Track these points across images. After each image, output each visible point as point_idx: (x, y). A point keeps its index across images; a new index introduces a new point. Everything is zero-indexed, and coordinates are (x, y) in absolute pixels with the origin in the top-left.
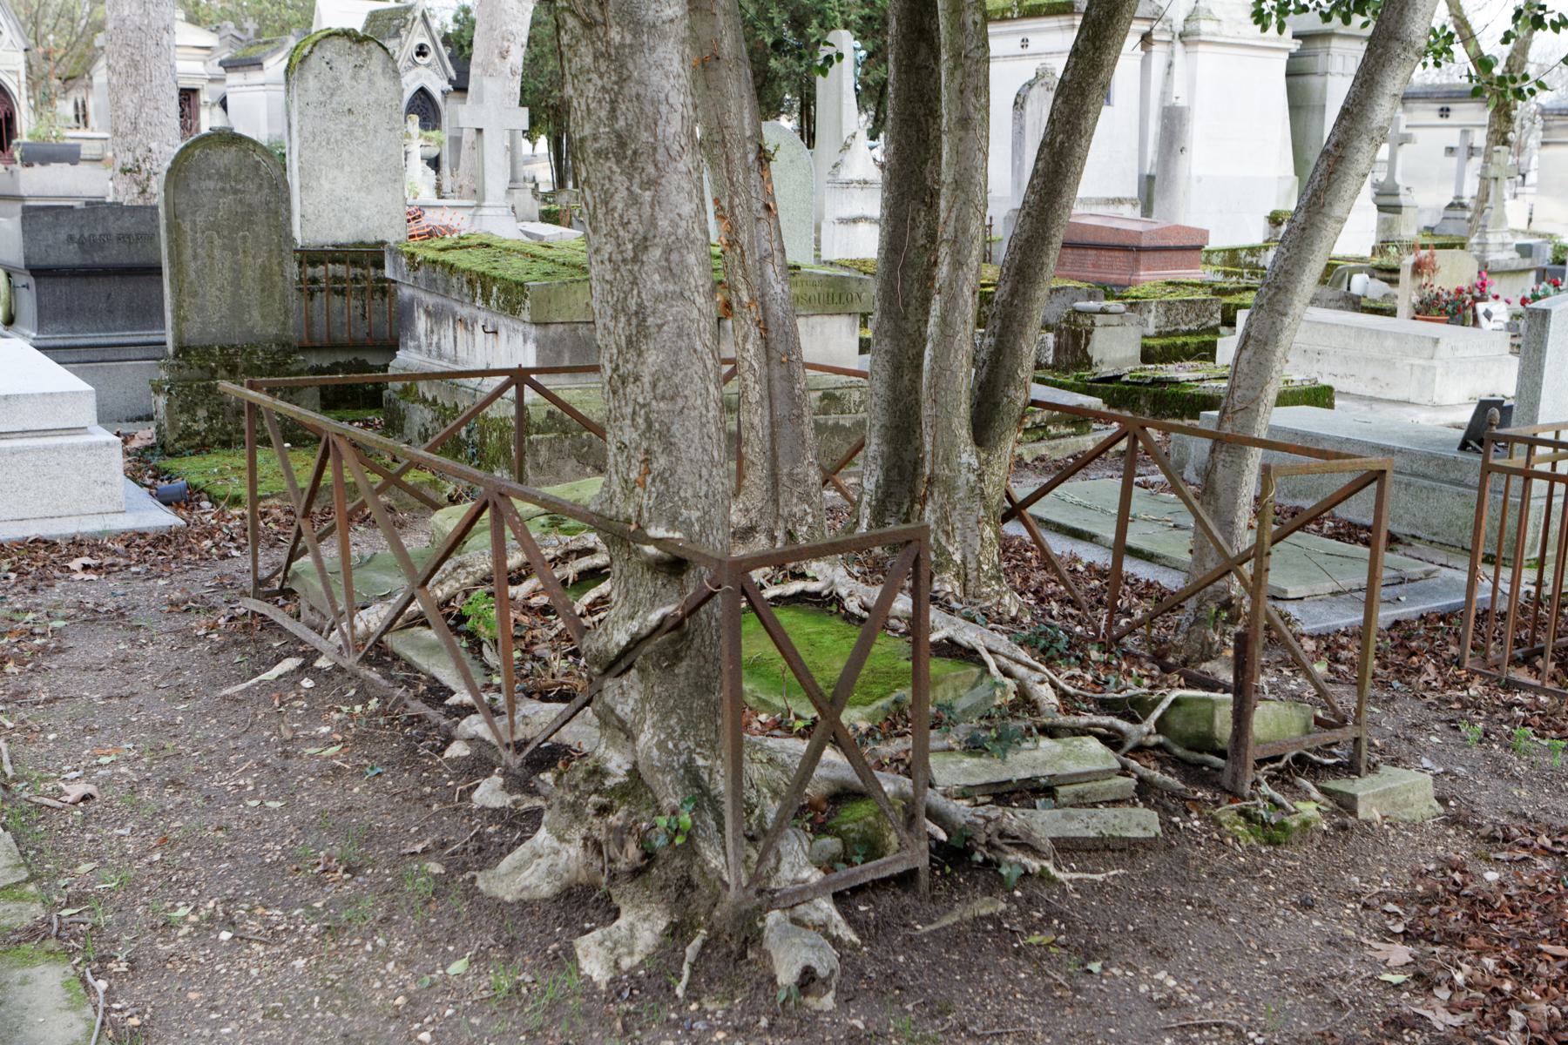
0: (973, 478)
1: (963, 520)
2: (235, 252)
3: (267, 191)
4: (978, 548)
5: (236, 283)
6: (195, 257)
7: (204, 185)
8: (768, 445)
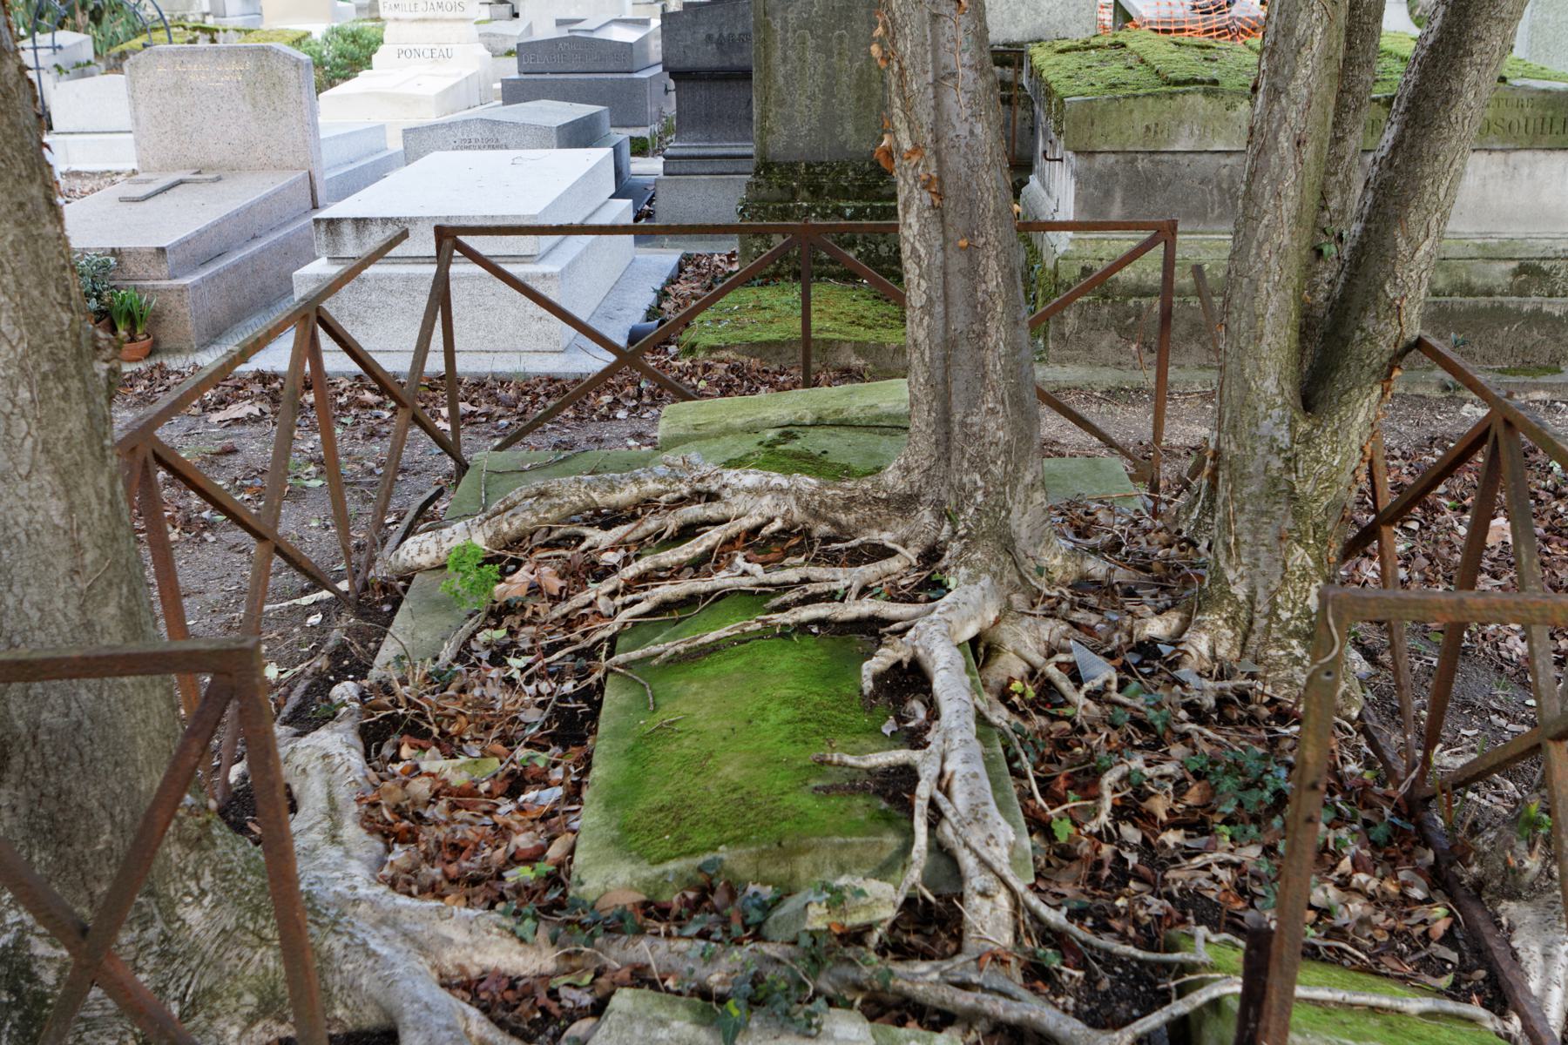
0: (1277, 463)
1: (1255, 532)
4: (1277, 582)
6: (785, 60)
8: (939, 374)
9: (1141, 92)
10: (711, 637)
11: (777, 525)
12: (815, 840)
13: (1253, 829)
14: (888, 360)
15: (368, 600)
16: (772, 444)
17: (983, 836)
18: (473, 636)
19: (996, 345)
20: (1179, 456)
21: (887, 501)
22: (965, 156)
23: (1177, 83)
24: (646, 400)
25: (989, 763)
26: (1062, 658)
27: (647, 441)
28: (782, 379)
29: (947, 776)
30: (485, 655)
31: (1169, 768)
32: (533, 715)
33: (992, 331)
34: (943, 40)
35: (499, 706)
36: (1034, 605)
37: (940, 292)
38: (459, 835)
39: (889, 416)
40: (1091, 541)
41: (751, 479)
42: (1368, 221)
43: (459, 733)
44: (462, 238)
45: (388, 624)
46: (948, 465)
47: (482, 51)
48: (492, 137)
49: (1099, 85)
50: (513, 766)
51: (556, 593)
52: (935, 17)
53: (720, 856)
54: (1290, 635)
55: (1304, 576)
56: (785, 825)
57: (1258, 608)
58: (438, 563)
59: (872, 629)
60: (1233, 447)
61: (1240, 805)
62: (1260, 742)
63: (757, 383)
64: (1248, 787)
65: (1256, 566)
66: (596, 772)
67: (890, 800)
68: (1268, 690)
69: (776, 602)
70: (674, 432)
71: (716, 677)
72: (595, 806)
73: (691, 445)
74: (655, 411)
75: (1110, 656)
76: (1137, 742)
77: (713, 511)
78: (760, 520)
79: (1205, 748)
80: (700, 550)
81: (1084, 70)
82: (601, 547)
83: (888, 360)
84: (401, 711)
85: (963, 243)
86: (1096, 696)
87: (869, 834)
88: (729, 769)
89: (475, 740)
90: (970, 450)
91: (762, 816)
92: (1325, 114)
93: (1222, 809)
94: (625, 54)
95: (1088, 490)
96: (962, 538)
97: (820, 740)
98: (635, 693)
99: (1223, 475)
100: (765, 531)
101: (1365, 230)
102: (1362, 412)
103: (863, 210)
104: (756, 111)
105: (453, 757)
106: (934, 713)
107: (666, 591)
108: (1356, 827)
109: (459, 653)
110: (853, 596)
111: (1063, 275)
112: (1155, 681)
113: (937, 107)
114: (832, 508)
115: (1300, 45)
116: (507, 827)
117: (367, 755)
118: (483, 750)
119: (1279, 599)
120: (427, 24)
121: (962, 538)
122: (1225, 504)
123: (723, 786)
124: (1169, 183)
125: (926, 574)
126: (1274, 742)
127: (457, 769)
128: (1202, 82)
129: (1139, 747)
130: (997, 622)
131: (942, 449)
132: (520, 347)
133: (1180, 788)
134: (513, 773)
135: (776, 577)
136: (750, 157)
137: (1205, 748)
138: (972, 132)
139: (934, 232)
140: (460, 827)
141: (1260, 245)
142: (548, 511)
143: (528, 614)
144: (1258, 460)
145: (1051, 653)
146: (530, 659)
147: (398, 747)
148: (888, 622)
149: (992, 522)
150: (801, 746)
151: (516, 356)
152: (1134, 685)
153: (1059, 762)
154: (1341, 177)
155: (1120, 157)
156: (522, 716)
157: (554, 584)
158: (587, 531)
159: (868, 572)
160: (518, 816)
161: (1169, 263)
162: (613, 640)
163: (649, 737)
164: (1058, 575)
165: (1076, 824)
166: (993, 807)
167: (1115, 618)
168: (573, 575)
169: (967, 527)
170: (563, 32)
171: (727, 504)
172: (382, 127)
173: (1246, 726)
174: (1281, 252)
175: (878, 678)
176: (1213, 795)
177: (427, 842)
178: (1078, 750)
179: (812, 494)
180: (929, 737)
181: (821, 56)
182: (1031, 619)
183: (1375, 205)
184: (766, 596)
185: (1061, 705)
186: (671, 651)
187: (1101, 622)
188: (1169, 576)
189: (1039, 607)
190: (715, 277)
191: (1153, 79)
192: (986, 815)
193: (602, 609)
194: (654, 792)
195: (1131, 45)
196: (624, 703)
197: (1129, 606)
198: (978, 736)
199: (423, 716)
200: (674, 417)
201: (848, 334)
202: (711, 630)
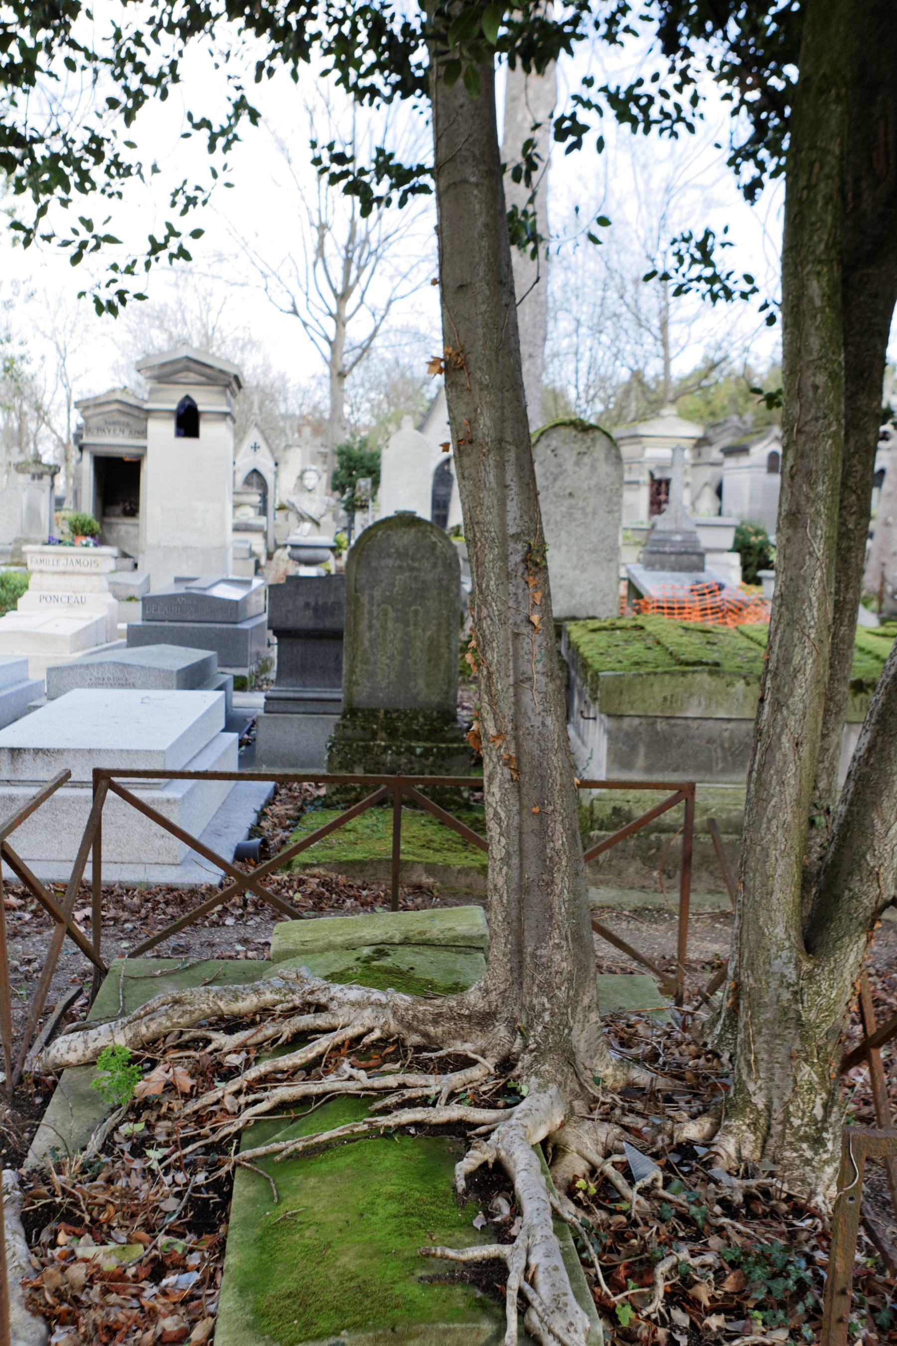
0: (786, 995)
1: (770, 1052)
2: (407, 624)
3: (440, 569)
4: (789, 1094)
5: (405, 653)
6: (370, 627)
7: (383, 562)
8: (514, 914)
9: (660, 670)
10: (325, 1136)
11: (377, 1034)
12: (423, 1326)
13: (781, 1315)
14: (453, 879)
15: (22, 1093)
16: (368, 960)
17: (564, 1324)
18: (116, 1129)
19: (562, 892)
20: (696, 970)
21: (469, 1017)
22: (538, 741)
23: (688, 664)
24: (251, 909)
25: (565, 1255)
26: (616, 1158)
27: (252, 946)
28: (364, 893)
29: (532, 1269)
30: (127, 1147)
31: (709, 1258)
32: (171, 1204)
33: (558, 880)
34: (522, 652)
35: (142, 1196)
36: (591, 1110)
37: (516, 848)
38: (112, 1318)
39: (464, 938)
40: (634, 1051)
41: (354, 993)
42: (851, 804)
43: (109, 1220)
44: (115, 779)
45: (40, 1115)
46: (521, 988)
47: (110, 599)
48: (122, 678)
49: (626, 663)
50: (155, 1252)
51: (188, 1090)
52: (516, 635)
53: (342, 1340)
54: (802, 1139)
55: (811, 1090)
56: (398, 1312)
57: (775, 1116)
58: (84, 1060)
59: (461, 1133)
60: (751, 981)
61: (770, 1292)
62: (781, 1234)
63: (343, 897)
64: (774, 1276)
65: (772, 1080)
66: (231, 1260)
67: (484, 1289)
68: (786, 1187)
69: (378, 1105)
70: (284, 947)
71: (330, 1172)
72: (230, 1291)
73: (299, 958)
74: (258, 919)
75: (656, 1156)
76: (681, 1234)
77: (322, 1020)
78: (361, 1030)
79: (737, 1240)
80: (312, 1055)
81: (613, 649)
82: (225, 1050)
83: (453, 879)
84: (58, 1200)
85: (536, 810)
86: (645, 1192)
87: (468, 1321)
88: (345, 1260)
89: (121, 1227)
90: (539, 978)
91: (376, 1304)
92: (816, 722)
93: (754, 1296)
94: (232, 610)
95: (627, 1003)
96: (532, 1051)
97: (422, 1233)
98: (260, 1186)
99: (743, 1004)
100: (367, 1040)
101: (849, 812)
102: (853, 956)
103: (431, 749)
104: (345, 667)
105: (103, 1243)
106: (517, 1210)
107: (283, 1092)
108: (864, 1312)
109: (104, 1144)
110: (443, 1101)
111: (598, 814)
112: (693, 1179)
113: (517, 703)
114: (423, 1022)
115: (796, 671)
116: (153, 1309)
117: (28, 1240)
118: (129, 1236)
119: (791, 1109)
120: (67, 577)
121: (532, 1051)
122: (746, 1027)
123: (342, 1275)
124: (682, 742)
125: (502, 1081)
126: (792, 1235)
127: (107, 1255)
128: (707, 664)
129: (682, 1239)
130: (562, 1125)
131: (515, 975)
132: (144, 860)
133: (719, 1275)
134: (156, 1258)
135: (378, 1082)
136: (339, 700)
137: (737, 1240)
138: (543, 724)
139: (513, 800)
140: (113, 1310)
141: (769, 821)
142: (181, 1017)
143: (164, 1109)
144: (772, 992)
145: (607, 1154)
146: (166, 1151)
147: (56, 1233)
148: (474, 1126)
149: (557, 1038)
150: (407, 1238)
151: (140, 868)
152: (676, 1183)
153: (619, 1252)
154: (827, 764)
155: (644, 721)
156: (162, 1205)
157: (186, 1083)
158: (213, 1035)
159: (455, 1079)
160: (162, 1300)
161: (689, 815)
162: (238, 1135)
163: (275, 1228)
164: (609, 1083)
165: (636, 1310)
166: (571, 1296)
167: (658, 1122)
168: (202, 1074)
169: (536, 1042)
170: (181, 589)
171: (334, 1015)
172: (26, 662)
173: (769, 1220)
174: (784, 825)
175: (469, 1177)
176: (746, 1282)
177: (87, 1325)
178: (634, 1241)
179: (407, 1009)
180: (514, 1231)
181: (400, 626)
182: (590, 1123)
183: (856, 793)
184: (371, 1099)
185: (617, 1201)
186: (291, 1148)
187: (647, 1125)
188: (699, 1085)
189: (597, 1112)
190: (305, 800)
191: (668, 659)
192: (566, 1305)
193: (228, 1107)
194: (282, 1280)
195: (649, 628)
196: (252, 1194)
197: (670, 1112)
198: (556, 1231)
199: (76, 1204)
200: (285, 934)
201: (420, 856)
202: (326, 1129)
